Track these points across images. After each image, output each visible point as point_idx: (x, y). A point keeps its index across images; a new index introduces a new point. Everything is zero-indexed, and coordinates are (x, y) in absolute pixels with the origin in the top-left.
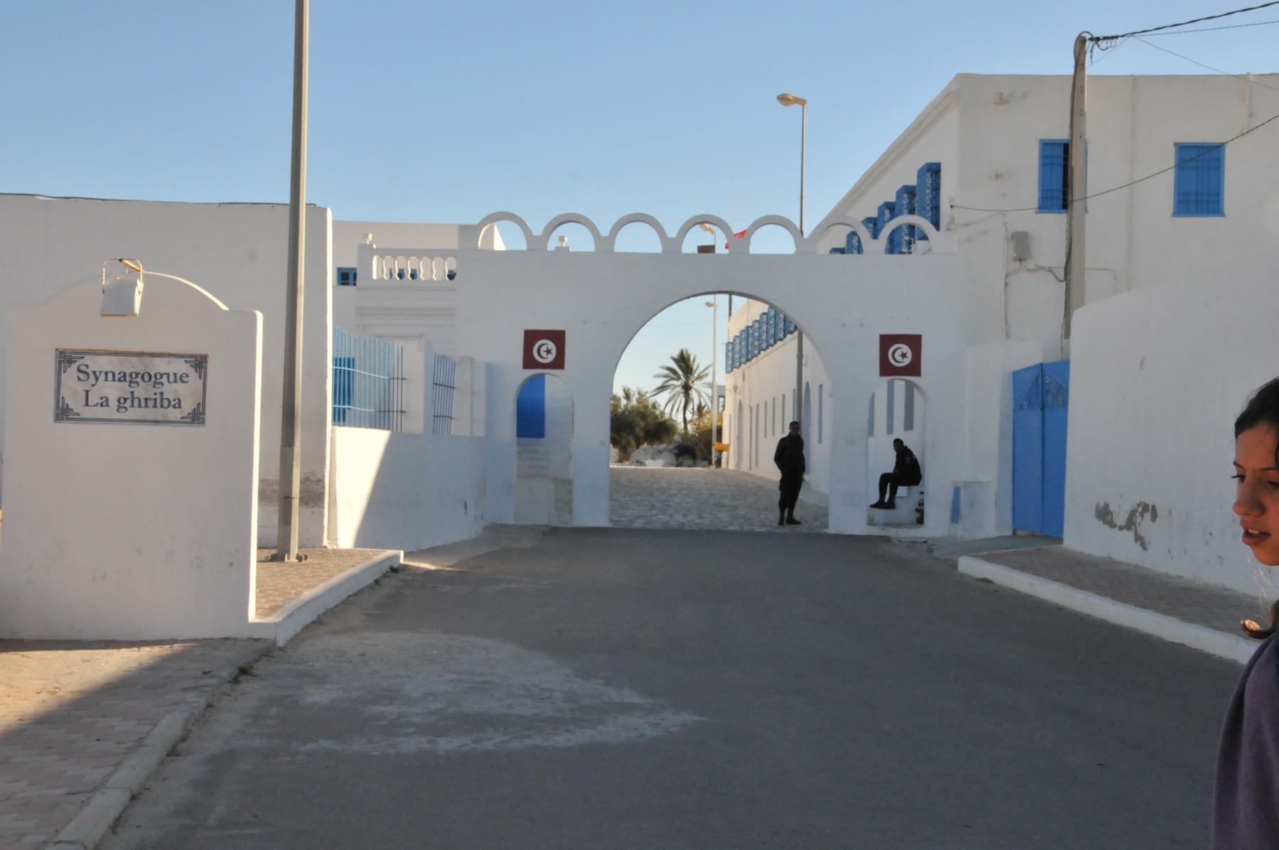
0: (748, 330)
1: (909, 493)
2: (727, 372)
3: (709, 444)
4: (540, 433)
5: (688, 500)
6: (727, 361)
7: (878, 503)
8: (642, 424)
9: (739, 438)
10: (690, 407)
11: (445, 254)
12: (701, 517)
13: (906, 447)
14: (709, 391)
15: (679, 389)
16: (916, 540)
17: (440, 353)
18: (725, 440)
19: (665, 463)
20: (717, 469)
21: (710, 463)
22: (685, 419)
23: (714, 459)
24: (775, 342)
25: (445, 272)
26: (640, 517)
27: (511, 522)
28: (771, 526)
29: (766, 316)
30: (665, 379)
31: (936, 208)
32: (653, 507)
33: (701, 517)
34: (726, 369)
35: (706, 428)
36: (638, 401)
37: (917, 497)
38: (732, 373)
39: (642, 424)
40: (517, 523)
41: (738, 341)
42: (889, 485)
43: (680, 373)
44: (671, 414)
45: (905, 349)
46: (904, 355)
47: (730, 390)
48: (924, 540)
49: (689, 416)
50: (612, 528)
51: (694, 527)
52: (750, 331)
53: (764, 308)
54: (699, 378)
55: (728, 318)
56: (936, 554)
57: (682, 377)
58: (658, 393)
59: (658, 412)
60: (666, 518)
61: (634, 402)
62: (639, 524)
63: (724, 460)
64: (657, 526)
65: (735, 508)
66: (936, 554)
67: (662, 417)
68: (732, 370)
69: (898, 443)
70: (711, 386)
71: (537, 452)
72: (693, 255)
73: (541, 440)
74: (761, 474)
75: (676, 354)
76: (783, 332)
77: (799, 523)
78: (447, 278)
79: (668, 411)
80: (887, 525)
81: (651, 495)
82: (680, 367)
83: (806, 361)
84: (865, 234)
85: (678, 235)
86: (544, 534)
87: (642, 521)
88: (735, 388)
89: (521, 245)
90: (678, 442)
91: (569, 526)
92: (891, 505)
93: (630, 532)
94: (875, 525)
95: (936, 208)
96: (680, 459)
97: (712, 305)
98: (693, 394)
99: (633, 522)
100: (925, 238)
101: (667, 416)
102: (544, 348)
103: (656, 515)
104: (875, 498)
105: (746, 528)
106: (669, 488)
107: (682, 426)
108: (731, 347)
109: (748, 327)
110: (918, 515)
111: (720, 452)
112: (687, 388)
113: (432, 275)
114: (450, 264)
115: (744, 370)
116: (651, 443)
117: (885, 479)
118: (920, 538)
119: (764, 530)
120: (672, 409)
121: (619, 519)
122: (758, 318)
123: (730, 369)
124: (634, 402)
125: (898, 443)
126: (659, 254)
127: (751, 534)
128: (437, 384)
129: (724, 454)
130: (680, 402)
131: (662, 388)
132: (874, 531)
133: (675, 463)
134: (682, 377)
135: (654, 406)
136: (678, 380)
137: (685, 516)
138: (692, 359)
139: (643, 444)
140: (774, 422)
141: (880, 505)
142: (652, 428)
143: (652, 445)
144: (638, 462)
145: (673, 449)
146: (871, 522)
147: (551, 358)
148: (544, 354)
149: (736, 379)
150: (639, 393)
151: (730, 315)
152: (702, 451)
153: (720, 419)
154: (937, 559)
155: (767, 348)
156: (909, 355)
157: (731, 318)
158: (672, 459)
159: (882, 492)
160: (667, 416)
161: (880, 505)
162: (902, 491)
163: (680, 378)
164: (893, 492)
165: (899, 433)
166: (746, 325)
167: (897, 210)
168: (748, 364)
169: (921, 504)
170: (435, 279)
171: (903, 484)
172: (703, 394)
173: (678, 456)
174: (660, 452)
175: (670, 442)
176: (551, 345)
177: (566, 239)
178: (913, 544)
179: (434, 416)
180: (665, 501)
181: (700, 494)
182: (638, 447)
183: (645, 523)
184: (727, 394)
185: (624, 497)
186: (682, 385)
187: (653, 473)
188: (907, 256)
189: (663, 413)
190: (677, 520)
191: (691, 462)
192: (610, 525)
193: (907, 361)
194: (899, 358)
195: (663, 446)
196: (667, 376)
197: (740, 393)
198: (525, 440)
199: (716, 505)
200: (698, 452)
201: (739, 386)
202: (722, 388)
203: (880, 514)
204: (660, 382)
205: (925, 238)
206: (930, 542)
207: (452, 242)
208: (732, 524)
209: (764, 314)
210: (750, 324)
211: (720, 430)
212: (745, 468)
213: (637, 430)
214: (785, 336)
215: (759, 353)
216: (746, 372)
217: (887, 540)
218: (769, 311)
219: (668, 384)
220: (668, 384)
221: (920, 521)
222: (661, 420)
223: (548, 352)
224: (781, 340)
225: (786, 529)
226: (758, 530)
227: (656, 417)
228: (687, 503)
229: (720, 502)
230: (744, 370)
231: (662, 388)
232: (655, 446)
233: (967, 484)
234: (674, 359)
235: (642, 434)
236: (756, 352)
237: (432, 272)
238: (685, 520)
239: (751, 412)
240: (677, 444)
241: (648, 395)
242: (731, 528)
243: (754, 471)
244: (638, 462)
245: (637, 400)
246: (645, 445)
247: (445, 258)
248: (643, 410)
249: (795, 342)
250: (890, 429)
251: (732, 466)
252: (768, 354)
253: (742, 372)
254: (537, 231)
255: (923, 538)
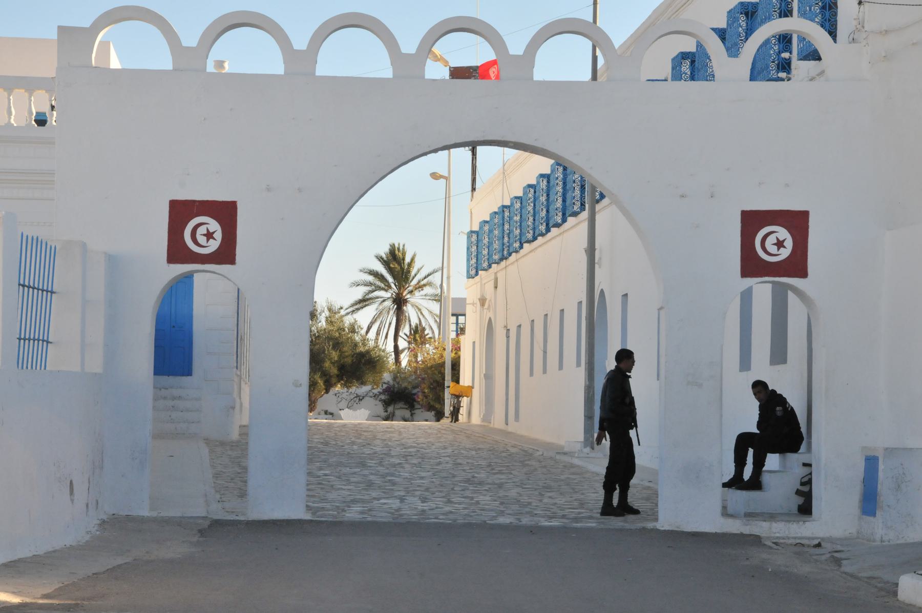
0: (503, 211)
1: (783, 464)
2: (470, 277)
3: (438, 386)
4: (187, 371)
5: (423, 474)
6: (468, 260)
7: (731, 480)
8: (335, 355)
9: (489, 377)
10: (405, 330)
11: (30, 85)
12: (449, 501)
13: (774, 391)
14: (435, 307)
15: (388, 303)
16: (803, 542)
17: (31, 232)
18: (465, 379)
19: (369, 416)
20: (453, 424)
21: (439, 416)
22: (396, 347)
23: (448, 409)
24: (548, 230)
25: (30, 113)
26: (354, 501)
27: (146, 513)
28: (564, 517)
29: (532, 191)
30: (363, 290)
31: (830, 8)
32: (370, 485)
33: (449, 501)
34: (468, 272)
35: (432, 362)
36: (329, 321)
37: (801, 472)
38: (477, 278)
39: (335, 355)
40: (154, 514)
41: (486, 228)
42: (751, 452)
43: (390, 279)
44: (377, 339)
45: (782, 233)
46: (780, 244)
47: (473, 304)
48: (816, 542)
49: (402, 344)
50: (311, 521)
51: (442, 519)
52: (507, 214)
53: (544, 165)
54: (419, 287)
55: (470, 193)
56: (847, 567)
57: (393, 286)
58: (358, 309)
59: (357, 338)
60: (395, 504)
61: (322, 323)
62: (353, 514)
63: (463, 411)
64: (383, 517)
65: (500, 486)
66: (847, 567)
67: (364, 345)
68: (477, 274)
69: (759, 387)
70: (438, 299)
71: (180, 398)
72: (443, 80)
73: (185, 380)
74: (523, 432)
75: (384, 251)
76: (560, 214)
77: (636, 512)
78: (34, 123)
79: (372, 335)
80: (750, 516)
81: (363, 465)
82: (391, 271)
83: (600, 259)
84: (715, 47)
85: (419, 48)
86: (201, 532)
87: (357, 508)
88: (483, 301)
89: (163, 61)
90: (388, 383)
91: (242, 518)
92: (755, 484)
93: (336, 526)
94: (731, 516)
95: (830, 8)
96: (390, 409)
97: (441, 177)
98: (409, 310)
99: (344, 510)
100: (814, 55)
101: (371, 344)
102: (202, 230)
103: (378, 499)
104: (729, 472)
105: (526, 521)
106: (388, 454)
107: (391, 359)
108: (475, 238)
109: (504, 207)
110: (800, 500)
111: (458, 397)
112: (399, 302)
113: (10, 118)
114: (39, 103)
115: (496, 273)
116: (347, 385)
117: (744, 442)
118: (809, 538)
119: (555, 523)
120: (378, 334)
121: (320, 505)
122: (520, 194)
123: (473, 272)
124: (322, 323)
125: (759, 387)
126: (388, 79)
127: (534, 530)
128: (24, 286)
129: (464, 401)
130: (390, 324)
131: (363, 302)
132: (734, 526)
133: (384, 414)
134: (393, 286)
135: (353, 330)
136: (386, 291)
137: (424, 500)
138: (408, 260)
139: (335, 384)
140: (545, 352)
141: (736, 483)
142: (349, 360)
143: (348, 387)
144: (326, 412)
145: (380, 393)
146: (726, 513)
147: (213, 246)
148: (202, 240)
149: (482, 286)
150: (330, 310)
151: (474, 189)
152: (426, 397)
153: (457, 348)
154: (845, 573)
155: (535, 239)
156: (789, 244)
157: (475, 193)
158: (380, 409)
159: (740, 462)
160: (371, 344)
161: (736, 483)
162: (772, 461)
163: (390, 287)
164: (759, 464)
165: (763, 370)
166: (500, 205)
167: (760, 14)
168: (503, 263)
169: (807, 482)
170: (15, 125)
171: (773, 452)
172: (425, 313)
173: (387, 404)
174: (360, 398)
175: (375, 383)
176: (214, 225)
177: (226, 65)
178: (800, 548)
179: (20, 339)
180: (388, 474)
181: (439, 463)
182: (327, 391)
183: (362, 513)
184: (469, 310)
185: (320, 469)
186: (392, 297)
187: (358, 430)
188: (786, 83)
189: (364, 341)
190: (412, 507)
191: (407, 413)
192: (308, 517)
193: (785, 253)
194: (771, 247)
195: (365, 389)
196: (370, 284)
197: (489, 308)
198: (155, 376)
199: (468, 481)
200: (420, 397)
201: (488, 297)
202: (461, 302)
203: (739, 497)
204: (359, 293)
205: (814, 55)
206: (827, 546)
207: (47, 67)
208: (502, 513)
209: (530, 186)
210: (508, 203)
211: (456, 366)
212: (498, 422)
213: (327, 364)
214: (564, 220)
215: (521, 247)
216: (499, 275)
217: (756, 540)
218: (538, 182)
219: (371, 295)
220: (371, 295)
221: (805, 509)
222: (362, 349)
223: (209, 235)
224: (557, 225)
225: (616, 522)
226: (545, 523)
227: (356, 345)
228: (422, 478)
229: (473, 477)
230: (496, 273)
231: (363, 302)
232: (353, 389)
233: (889, 451)
234: (380, 259)
235: (334, 371)
236: (517, 245)
237: (10, 113)
238: (425, 507)
239: (508, 337)
240: (385, 386)
241: (343, 312)
242: (502, 520)
243: (513, 427)
244: (326, 412)
245: (327, 320)
246: (338, 388)
247: (30, 92)
248: (337, 335)
249: (584, 227)
250: (745, 363)
251: (476, 419)
252: (536, 248)
253: (493, 277)
254: (190, 38)
255: (813, 539)
